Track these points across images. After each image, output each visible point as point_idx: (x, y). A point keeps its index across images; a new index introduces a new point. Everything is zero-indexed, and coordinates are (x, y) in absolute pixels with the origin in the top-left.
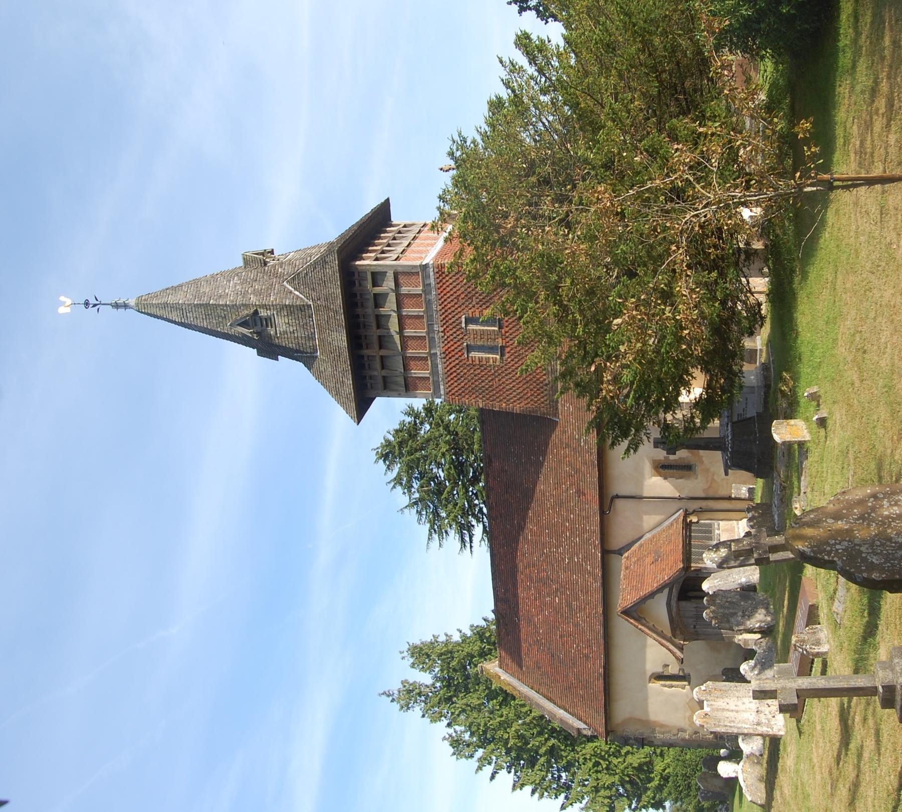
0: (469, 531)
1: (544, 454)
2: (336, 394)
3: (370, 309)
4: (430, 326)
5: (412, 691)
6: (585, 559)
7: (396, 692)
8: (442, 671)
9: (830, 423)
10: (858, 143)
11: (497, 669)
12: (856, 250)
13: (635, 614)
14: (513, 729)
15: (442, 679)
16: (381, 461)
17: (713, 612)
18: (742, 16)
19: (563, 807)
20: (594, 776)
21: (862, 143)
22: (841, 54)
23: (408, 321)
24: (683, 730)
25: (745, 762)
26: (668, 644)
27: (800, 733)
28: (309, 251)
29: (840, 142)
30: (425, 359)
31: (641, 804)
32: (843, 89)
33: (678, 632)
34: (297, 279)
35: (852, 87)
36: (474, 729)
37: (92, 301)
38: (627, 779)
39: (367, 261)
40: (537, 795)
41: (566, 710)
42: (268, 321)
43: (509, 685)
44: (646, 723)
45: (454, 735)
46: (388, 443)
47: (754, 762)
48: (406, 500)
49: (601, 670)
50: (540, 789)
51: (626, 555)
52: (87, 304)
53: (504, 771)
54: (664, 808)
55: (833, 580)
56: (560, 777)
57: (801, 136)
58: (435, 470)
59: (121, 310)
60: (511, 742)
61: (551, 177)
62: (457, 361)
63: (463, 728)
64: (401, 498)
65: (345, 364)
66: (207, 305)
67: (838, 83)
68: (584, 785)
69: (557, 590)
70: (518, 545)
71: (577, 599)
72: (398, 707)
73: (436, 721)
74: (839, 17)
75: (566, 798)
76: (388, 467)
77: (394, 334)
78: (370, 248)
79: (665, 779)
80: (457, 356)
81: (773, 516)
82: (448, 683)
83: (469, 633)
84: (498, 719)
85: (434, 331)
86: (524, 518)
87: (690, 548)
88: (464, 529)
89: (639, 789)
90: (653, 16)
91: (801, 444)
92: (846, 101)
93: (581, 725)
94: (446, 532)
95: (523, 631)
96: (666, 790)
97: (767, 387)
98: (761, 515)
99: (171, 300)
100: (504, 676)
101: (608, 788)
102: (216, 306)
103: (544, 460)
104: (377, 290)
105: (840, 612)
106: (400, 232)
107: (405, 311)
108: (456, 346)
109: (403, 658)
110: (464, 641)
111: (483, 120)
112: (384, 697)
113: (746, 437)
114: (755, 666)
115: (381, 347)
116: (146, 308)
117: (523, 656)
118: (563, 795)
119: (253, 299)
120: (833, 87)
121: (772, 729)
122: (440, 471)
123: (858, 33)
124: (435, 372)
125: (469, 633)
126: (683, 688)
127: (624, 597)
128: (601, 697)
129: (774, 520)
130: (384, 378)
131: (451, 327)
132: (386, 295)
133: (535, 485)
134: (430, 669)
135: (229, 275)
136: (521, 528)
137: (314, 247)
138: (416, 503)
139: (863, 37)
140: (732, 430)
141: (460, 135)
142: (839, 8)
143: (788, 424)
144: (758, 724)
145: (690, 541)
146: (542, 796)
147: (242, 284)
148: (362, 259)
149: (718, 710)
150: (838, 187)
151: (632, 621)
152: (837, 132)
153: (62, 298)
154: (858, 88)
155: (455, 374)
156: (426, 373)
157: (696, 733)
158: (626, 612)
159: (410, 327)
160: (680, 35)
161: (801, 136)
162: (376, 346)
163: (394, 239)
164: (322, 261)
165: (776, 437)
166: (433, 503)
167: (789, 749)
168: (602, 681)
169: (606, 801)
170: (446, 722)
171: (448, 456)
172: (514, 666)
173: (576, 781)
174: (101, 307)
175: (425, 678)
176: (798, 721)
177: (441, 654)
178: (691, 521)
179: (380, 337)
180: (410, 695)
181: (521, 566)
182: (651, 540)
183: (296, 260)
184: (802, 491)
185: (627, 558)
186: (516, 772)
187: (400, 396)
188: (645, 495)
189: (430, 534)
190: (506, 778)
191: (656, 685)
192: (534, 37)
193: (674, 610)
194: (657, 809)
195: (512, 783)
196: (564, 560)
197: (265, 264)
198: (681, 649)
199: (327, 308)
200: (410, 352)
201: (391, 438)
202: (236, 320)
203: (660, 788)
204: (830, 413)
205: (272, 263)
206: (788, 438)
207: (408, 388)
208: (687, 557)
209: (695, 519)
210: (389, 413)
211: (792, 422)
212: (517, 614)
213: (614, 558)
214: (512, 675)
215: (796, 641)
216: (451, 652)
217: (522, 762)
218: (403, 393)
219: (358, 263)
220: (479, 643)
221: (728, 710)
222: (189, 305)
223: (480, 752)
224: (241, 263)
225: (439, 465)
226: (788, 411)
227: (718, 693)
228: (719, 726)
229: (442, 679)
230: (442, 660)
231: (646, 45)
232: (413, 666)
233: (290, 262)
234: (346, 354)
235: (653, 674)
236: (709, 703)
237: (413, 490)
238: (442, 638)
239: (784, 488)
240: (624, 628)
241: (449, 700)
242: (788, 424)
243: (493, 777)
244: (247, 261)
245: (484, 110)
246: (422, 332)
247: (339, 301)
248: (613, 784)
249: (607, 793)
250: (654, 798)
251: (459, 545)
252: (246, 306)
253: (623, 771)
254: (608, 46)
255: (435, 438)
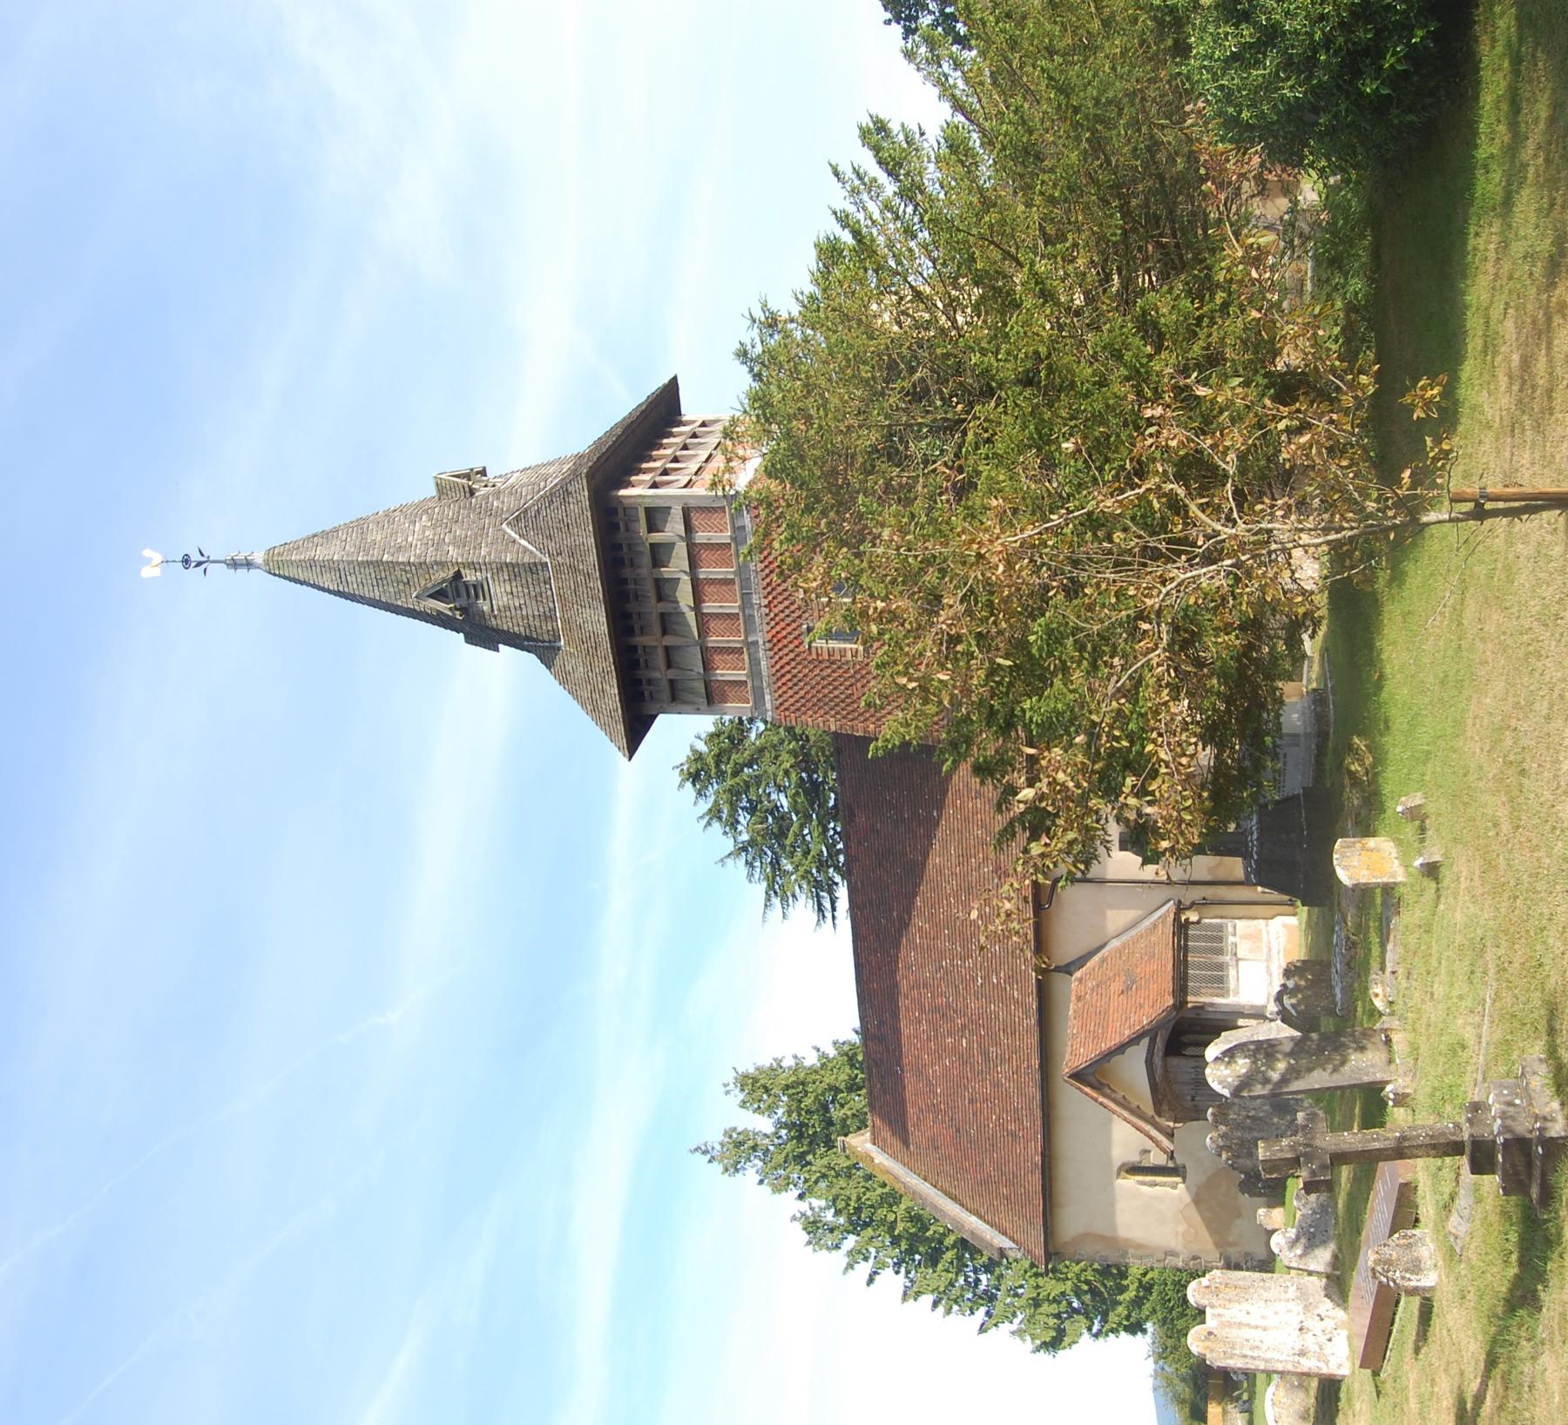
0: (831, 892)
1: (940, 806)
2: (594, 709)
3: (645, 570)
4: (746, 597)
5: (741, 1144)
6: (1010, 979)
7: (718, 1147)
8: (789, 1113)
9: (1445, 872)
10: (1516, 357)
11: (869, 1146)
12: (1508, 568)
13: (1093, 1080)
14: (903, 1206)
15: (789, 1126)
16: (689, 785)
17: (1222, 1136)
18: (1282, 98)
19: (983, 1329)
20: (1032, 1281)
21: (1526, 362)
22: (1479, 173)
23: (708, 589)
24: (1174, 1254)
25: (1277, 1386)
26: (1148, 1127)
27: (1378, 1393)
28: (543, 471)
29: (1474, 344)
30: (739, 651)
31: (1107, 1327)
32: (1483, 240)
33: (1165, 1107)
34: (523, 519)
35: (1504, 245)
36: (841, 1205)
37: (196, 557)
38: (1085, 1288)
39: (637, 490)
40: (941, 1309)
41: (980, 1217)
42: (478, 589)
43: (888, 1172)
44: (1112, 1241)
45: (809, 1213)
46: (698, 757)
47: (1292, 1386)
48: (729, 845)
49: (1038, 1159)
50: (945, 1299)
51: (1078, 974)
52: (186, 561)
53: (889, 1272)
54: (1144, 1331)
55: (1447, 1174)
56: (977, 1281)
57: (1419, 414)
58: (774, 796)
59: (242, 572)
60: (900, 1227)
61: (931, 391)
62: (792, 655)
63: (823, 1203)
64: (719, 841)
65: (606, 662)
66: (378, 564)
67: (1472, 229)
68: (1016, 1295)
69: (964, 1027)
70: (898, 951)
71: (998, 1044)
72: (721, 1168)
73: (779, 1191)
74: (1476, 98)
75: (988, 1314)
76: (699, 793)
77: (685, 609)
78: (644, 465)
79: (1147, 1288)
80: (791, 646)
81: (1332, 987)
82: (798, 1130)
83: (832, 1053)
84: (880, 1191)
85: (752, 605)
86: (908, 909)
87: (1186, 968)
88: (821, 888)
89: (1104, 1301)
90: (1110, 94)
91: (1388, 889)
92: (1489, 266)
93: (1005, 1243)
94: (794, 896)
95: (909, 1088)
96: (1147, 1306)
97: (1322, 735)
98: (1312, 984)
99: (320, 553)
100: (881, 1158)
101: (1055, 1300)
102: (393, 565)
103: (940, 816)
104: (656, 537)
105: (1461, 1234)
106: (694, 436)
107: (703, 573)
108: (789, 629)
109: (727, 1093)
110: (823, 1065)
111: (808, 278)
112: (698, 1154)
113: (1283, 836)
114: (1298, 1238)
115: (664, 632)
116: (281, 566)
117: (911, 1129)
118: (983, 1310)
119: (453, 553)
120: (1462, 235)
121: (1327, 1363)
122: (782, 796)
123: (1517, 138)
124: (755, 672)
125: (832, 1053)
126: (1174, 1187)
127: (1075, 1051)
128: (1038, 1201)
129: (1334, 996)
130: (671, 682)
131: (780, 598)
132: (671, 546)
133: (926, 855)
134: (771, 1110)
135: (414, 512)
136: (904, 924)
137: (551, 464)
138: (744, 849)
139: (1530, 145)
140: (1260, 821)
141: (764, 307)
142: (1479, 82)
143: (1363, 848)
144: (1302, 1353)
145: (1185, 956)
146: (949, 1311)
147: (434, 527)
148: (629, 484)
149: (1230, 1325)
150: (1495, 513)
151: (1087, 1090)
152: (1470, 324)
153: (147, 553)
154: (1518, 248)
155: (789, 676)
156: (740, 675)
157: (1194, 1258)
158: (1078, 1076)
159: (716, 598)
160: (1163, 127)
161: (1419, 414)
162: (657, 630)
163: (685, 447)
164: (562, 492)
165: (1343, 875)
166: (771, 848)
167: (1357, 1406)
168: (1038, 1175)
169: (1052, 1322)
170: (796, 1192)
171: (793, 776)
172: (897, 1144)
173: (1003, 1287)
174: (210, 567)
175: (764, 1124)
176: (1376, 1374)
177: (787, 1087)
178: (1187, 920)
179: (662, 615)
180: (739, 1149)
181: (904, 985)
182: (1120, 951)
183: (522, 486)
184: (1389, 969)
185: (1080, 980)
186: (908, 1272)
187: (698, 711)
188: (1110, 876)
189: (768, 898)
190: (892, 1282)
191: (1130, 1182)
192: (895, 127)
193: (1159, 1071)
194: (1134, 1333)
195: (902, 1289)
196: (974, 979)
197: (472, 492)
198: (1170, 1135)
199: (573, 569)
200: (713, 640)
201: (702, 747)
202: (427, 589)
203: (1138, 1302)
204: (1446, 855)
205: (483, 491)
206: (1364, 877)
207: (712, 697)
208: (1181, 986)
209: (1194, 917)
210: (679, 733)
211: (1371, 842)
212: (899, 1062)
213: (1059, 978)
214: (893, 1156)
215: (1377, 1262)
216: (803, 1084)
217: (917, 1257)
218: (704, 707)
219: (622, 492)
220: (847, 1069)
221: (1248, 1325)
222: (349, 563)
223: (851, 1241)
224: (433, 492)
225: (780, 789)
226: (1364, 812)
227: (1231, 1293)
228: (1232, 1356)
229: (789, 1126)
230: (790, 1096)
231: (1098, 146)
232: (743, 1104)
233: (513, 491)
234: (606, 644)
235: (1123, 1165)
236: (1216, 1311)
237: (740, 828)
238: (788, 1062)
239: (1354, 944)
240: (1075, 1102)
241: (801, 1159)
242: (1363, 848)
243: (871, 1281)
244: (442, 488)
245: (810, 260)
246: (733, 607)
247: (593, 558)
248: (1063, 1294)
249: (1053, 1308)
250: (1128, 1317)
251: (814, 916)
252: (442, 564)
253: (1078, 1276)
254: (1026, 152)
255: (774, 746)
